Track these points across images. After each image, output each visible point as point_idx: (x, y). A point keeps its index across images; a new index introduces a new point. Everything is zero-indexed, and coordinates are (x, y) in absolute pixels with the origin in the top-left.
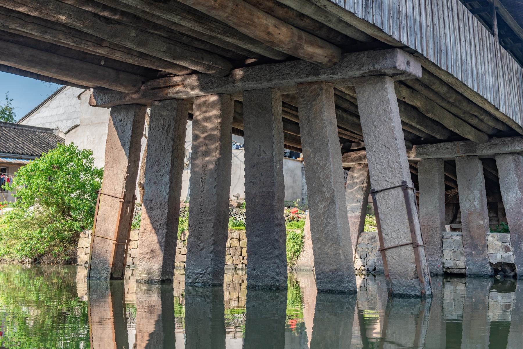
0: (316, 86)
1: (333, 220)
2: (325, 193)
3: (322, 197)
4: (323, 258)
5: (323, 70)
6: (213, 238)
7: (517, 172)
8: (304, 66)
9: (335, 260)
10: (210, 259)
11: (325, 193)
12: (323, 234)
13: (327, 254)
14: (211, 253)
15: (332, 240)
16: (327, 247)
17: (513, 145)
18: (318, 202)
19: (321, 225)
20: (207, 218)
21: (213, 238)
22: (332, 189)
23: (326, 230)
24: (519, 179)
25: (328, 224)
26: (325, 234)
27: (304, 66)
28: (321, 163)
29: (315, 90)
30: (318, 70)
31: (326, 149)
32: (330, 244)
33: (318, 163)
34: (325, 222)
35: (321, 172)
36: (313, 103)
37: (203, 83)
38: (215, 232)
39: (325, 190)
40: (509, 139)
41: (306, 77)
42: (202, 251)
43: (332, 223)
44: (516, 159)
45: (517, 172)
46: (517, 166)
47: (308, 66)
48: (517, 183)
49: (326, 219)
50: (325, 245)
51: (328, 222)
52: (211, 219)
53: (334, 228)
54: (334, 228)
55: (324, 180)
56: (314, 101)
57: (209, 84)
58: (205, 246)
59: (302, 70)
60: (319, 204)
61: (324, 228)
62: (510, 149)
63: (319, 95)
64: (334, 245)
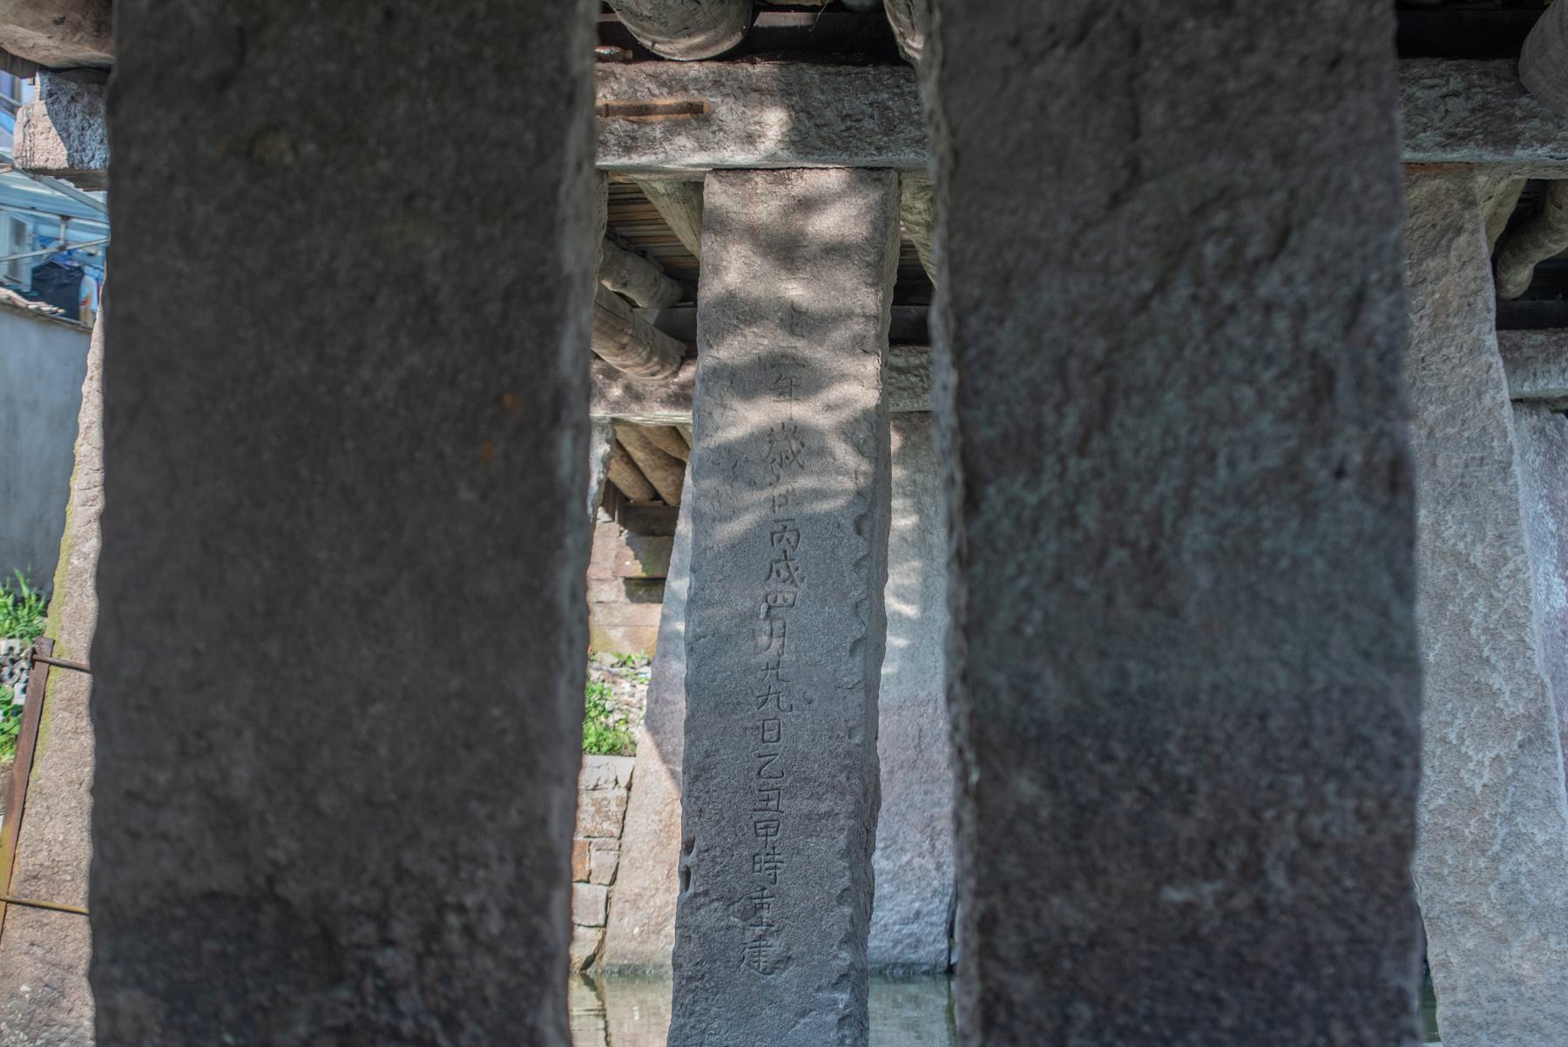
0: (1441, 183)
1: (1542, 825)
2: (1495, 694)
3: (1482, 714)
4: (1493, 999)
5: (1536, 123)
6: (847, 910)
7: (1552, 489)
8: (1435, 93)
9: (1556, 1008)
10: (832, 1018)
11: (1495, 694)
12: (1492, 889)
13: (1516, 982)
14: (835, 986)
15: (1536, 915)
16: (1517, 949)
17: (1554, 369)
18: (1461, 739)
19: (1480, 846)
20: (804, 805)
21: (847, 910)
22: (1531, 678)
23: (1505, 871)
24: (1560, 523)
25: (1518, 839)
26: (1502, 887)
27: (1435, 93)
28: (1478, 555)
29: (1433, 200)
30: (1508, 119)
31: (1501, 489)
32: (1532, 933)
33: (1456, 555)
34: (1502, 832)
35: (1473, 598)
36: (1432, 264)
37: (829, 114)
38: (853, 880)
39: (1497, 681)
40: (1539, 337)
41: (1444, 146)
42: (779, 979)
43: (1540, 838)
44: (1550, 428)
45: (1552, 489)
46: (1554, 462)
47: (1455, 94)
48: (1554, 543)
49: (1508, 819)
50: (1504, 941)
51: (1519, 835)
52: (828, 814)
53: (1548, 859)
54: (1548, 863)
55: (1493, 635)
56: (1432, 251)
57: (868, 124)
58: (795, 951)
59: (1422, 111)
60: (1469, 748)
61: (1496, 859)
62: (1541, 383)
63: (1459, 231)
64: (1553, 940)
